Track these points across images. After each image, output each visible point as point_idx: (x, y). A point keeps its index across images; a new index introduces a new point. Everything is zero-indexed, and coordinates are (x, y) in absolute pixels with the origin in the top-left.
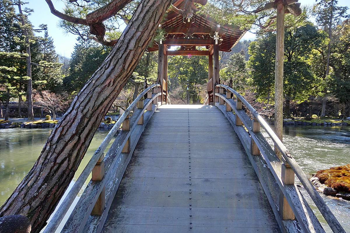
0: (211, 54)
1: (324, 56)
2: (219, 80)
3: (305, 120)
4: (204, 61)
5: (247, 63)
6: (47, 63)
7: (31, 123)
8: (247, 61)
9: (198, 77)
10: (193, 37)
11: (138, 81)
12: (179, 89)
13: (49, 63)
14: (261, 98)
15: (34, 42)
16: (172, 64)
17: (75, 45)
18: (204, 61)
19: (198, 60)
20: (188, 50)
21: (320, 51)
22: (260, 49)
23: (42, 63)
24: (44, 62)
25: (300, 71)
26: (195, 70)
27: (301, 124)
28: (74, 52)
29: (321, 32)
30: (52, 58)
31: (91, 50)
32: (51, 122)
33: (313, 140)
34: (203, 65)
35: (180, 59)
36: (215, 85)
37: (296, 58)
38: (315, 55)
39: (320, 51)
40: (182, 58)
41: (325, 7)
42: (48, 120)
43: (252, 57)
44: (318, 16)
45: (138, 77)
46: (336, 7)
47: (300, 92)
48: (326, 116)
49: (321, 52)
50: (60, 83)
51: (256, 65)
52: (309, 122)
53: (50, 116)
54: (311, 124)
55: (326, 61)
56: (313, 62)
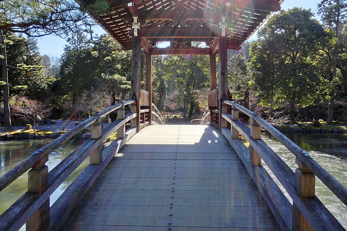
0: (213, 53)
1: (330, 57)
2: (227, 92)
3: (314, 126)
4: (202, 62)
5: (249, 65)
6: (25, 66)
7: (8, 133)
8: (248, 63)
9: (196, 79)
10: (186, 26)
11: (125, 87)
12: (176, 93)
13: (28, 66)
14: (263, 102)
15: (11, 42)
16: (168, 66)
17: (65, 47)
18: (202, 62)
19: (196, 62)
20: (181, 47)
21: (325, 52)
22: (262, 50)
23: (19, 66)
24: (22, 65)
25: (306, 74)
26: (192, 73)
27: (309, 131)
28: (64, 54)
29: (328, 31)
30: (35, 60)
31: (81, 52)
32: (30, 133)
33: (333, 156)
34: (201, 67)
35: (177, 60)
36: (222, 100)
37: (301, 59)
38: (322, 55)
39: (325, 52)
40: (179, 59)
41: (329, 6)
42: (28, 129)
43: (254, 59)
44: (323, 14)
45: (125, 81)
46: (344, 4)
47: (306, 95)
48: (333, 121)
49: (327, 53)
50: (44, 88)
51: (258, 66)
52: (318, 128)
53: (31, 126)
54: (320, 131)
55: (333, 61)
56: (318, 63)
